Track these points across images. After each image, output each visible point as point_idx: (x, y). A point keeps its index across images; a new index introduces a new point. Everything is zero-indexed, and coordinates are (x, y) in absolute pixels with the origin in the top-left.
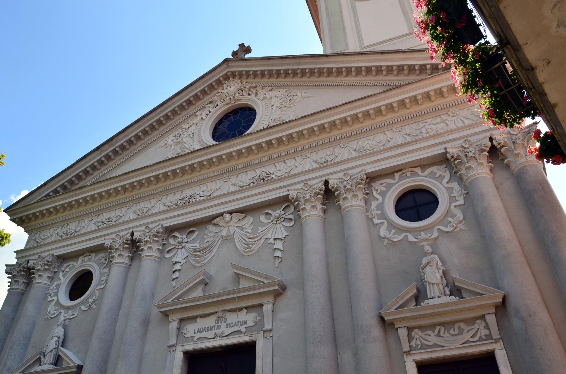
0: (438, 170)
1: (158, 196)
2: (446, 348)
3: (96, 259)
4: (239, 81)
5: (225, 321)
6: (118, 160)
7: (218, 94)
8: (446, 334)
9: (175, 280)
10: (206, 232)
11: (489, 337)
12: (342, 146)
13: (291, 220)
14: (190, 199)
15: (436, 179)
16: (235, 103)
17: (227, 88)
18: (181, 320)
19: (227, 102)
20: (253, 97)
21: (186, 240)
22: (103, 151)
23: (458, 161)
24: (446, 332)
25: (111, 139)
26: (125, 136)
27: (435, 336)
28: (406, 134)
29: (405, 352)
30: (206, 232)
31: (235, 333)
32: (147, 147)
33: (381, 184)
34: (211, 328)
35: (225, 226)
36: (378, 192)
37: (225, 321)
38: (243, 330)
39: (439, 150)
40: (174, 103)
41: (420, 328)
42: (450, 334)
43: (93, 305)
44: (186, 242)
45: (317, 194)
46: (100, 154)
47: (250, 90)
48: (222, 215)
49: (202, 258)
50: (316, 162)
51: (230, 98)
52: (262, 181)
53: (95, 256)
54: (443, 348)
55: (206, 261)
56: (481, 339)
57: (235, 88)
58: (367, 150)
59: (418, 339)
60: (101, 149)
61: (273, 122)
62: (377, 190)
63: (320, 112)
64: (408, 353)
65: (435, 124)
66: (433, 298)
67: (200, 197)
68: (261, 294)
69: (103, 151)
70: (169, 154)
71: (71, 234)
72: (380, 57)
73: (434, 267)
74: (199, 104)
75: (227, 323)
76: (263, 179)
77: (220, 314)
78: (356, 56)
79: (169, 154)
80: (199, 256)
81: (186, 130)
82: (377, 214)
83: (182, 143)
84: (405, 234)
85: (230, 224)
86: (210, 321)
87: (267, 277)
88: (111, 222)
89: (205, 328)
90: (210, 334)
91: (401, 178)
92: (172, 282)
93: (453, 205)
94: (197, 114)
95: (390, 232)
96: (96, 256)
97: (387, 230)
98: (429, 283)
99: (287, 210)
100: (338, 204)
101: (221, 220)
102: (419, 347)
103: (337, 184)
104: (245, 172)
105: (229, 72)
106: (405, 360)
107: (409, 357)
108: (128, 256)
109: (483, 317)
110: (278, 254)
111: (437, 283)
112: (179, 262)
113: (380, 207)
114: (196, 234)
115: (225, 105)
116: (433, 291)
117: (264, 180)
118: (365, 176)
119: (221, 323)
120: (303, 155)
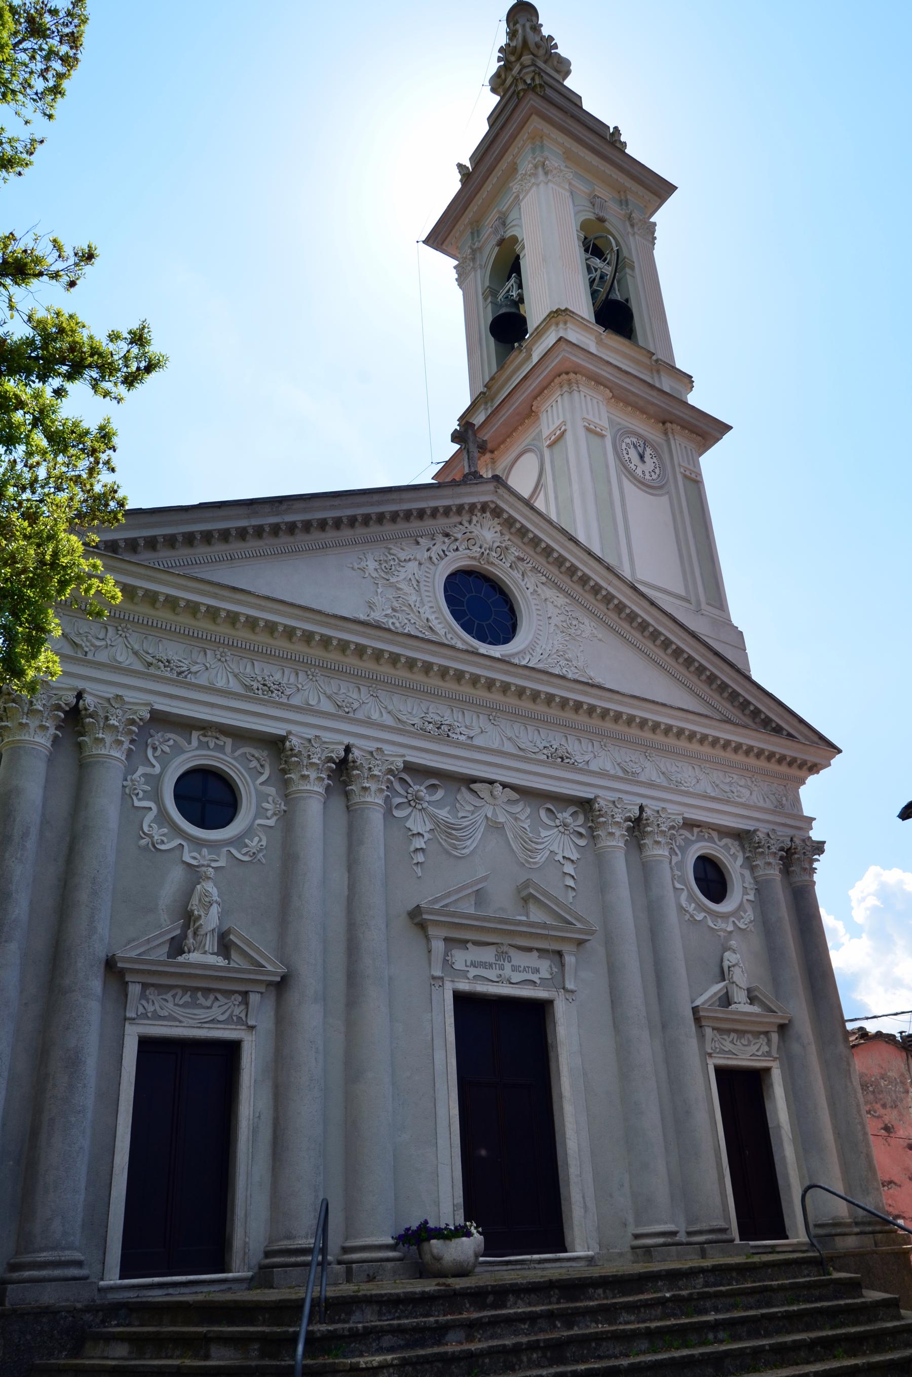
1: (374, 686)
4: (498, 528)
6: (267, 544)
7: (460, 526)
8: (738, 1043)
11: (768, 1054)
13: (580, 835)
18: (446, 940)
20: (516, 575)
21: (427, 798)
23: (14, 705)
30: (459, 797)
31: (527, 982)
32: (325, 547)
34: (491, 965)
36: (156, 755)
38: (538, 981)
39: (277, 729)
48: (491, 782)
52: (560, 760)
56: (763, 1055)
63: (653, 702)
64: (710, 1055)
66: (739, 1003)
68: (563, 939)
70: (376, 597)
71: (179, 674)
76: (562, 758)
77: (505, 949)
78: (685, 633)
80: (457, 839)
84: (703, 914)
86: (488, 955)
87: (579, 919)
90: (492, 974)
91: (203, 745)
93: (259, 821)
95: (690, 905)
98: (737, 985)
102: (718, 1050)
103: (95, 707)
104: (525, 725)
105: (492, 502)
109: (766, 1033)
110: (571, 883)
114: (440, 794)
117: (563, 759)
118: (681, 821)
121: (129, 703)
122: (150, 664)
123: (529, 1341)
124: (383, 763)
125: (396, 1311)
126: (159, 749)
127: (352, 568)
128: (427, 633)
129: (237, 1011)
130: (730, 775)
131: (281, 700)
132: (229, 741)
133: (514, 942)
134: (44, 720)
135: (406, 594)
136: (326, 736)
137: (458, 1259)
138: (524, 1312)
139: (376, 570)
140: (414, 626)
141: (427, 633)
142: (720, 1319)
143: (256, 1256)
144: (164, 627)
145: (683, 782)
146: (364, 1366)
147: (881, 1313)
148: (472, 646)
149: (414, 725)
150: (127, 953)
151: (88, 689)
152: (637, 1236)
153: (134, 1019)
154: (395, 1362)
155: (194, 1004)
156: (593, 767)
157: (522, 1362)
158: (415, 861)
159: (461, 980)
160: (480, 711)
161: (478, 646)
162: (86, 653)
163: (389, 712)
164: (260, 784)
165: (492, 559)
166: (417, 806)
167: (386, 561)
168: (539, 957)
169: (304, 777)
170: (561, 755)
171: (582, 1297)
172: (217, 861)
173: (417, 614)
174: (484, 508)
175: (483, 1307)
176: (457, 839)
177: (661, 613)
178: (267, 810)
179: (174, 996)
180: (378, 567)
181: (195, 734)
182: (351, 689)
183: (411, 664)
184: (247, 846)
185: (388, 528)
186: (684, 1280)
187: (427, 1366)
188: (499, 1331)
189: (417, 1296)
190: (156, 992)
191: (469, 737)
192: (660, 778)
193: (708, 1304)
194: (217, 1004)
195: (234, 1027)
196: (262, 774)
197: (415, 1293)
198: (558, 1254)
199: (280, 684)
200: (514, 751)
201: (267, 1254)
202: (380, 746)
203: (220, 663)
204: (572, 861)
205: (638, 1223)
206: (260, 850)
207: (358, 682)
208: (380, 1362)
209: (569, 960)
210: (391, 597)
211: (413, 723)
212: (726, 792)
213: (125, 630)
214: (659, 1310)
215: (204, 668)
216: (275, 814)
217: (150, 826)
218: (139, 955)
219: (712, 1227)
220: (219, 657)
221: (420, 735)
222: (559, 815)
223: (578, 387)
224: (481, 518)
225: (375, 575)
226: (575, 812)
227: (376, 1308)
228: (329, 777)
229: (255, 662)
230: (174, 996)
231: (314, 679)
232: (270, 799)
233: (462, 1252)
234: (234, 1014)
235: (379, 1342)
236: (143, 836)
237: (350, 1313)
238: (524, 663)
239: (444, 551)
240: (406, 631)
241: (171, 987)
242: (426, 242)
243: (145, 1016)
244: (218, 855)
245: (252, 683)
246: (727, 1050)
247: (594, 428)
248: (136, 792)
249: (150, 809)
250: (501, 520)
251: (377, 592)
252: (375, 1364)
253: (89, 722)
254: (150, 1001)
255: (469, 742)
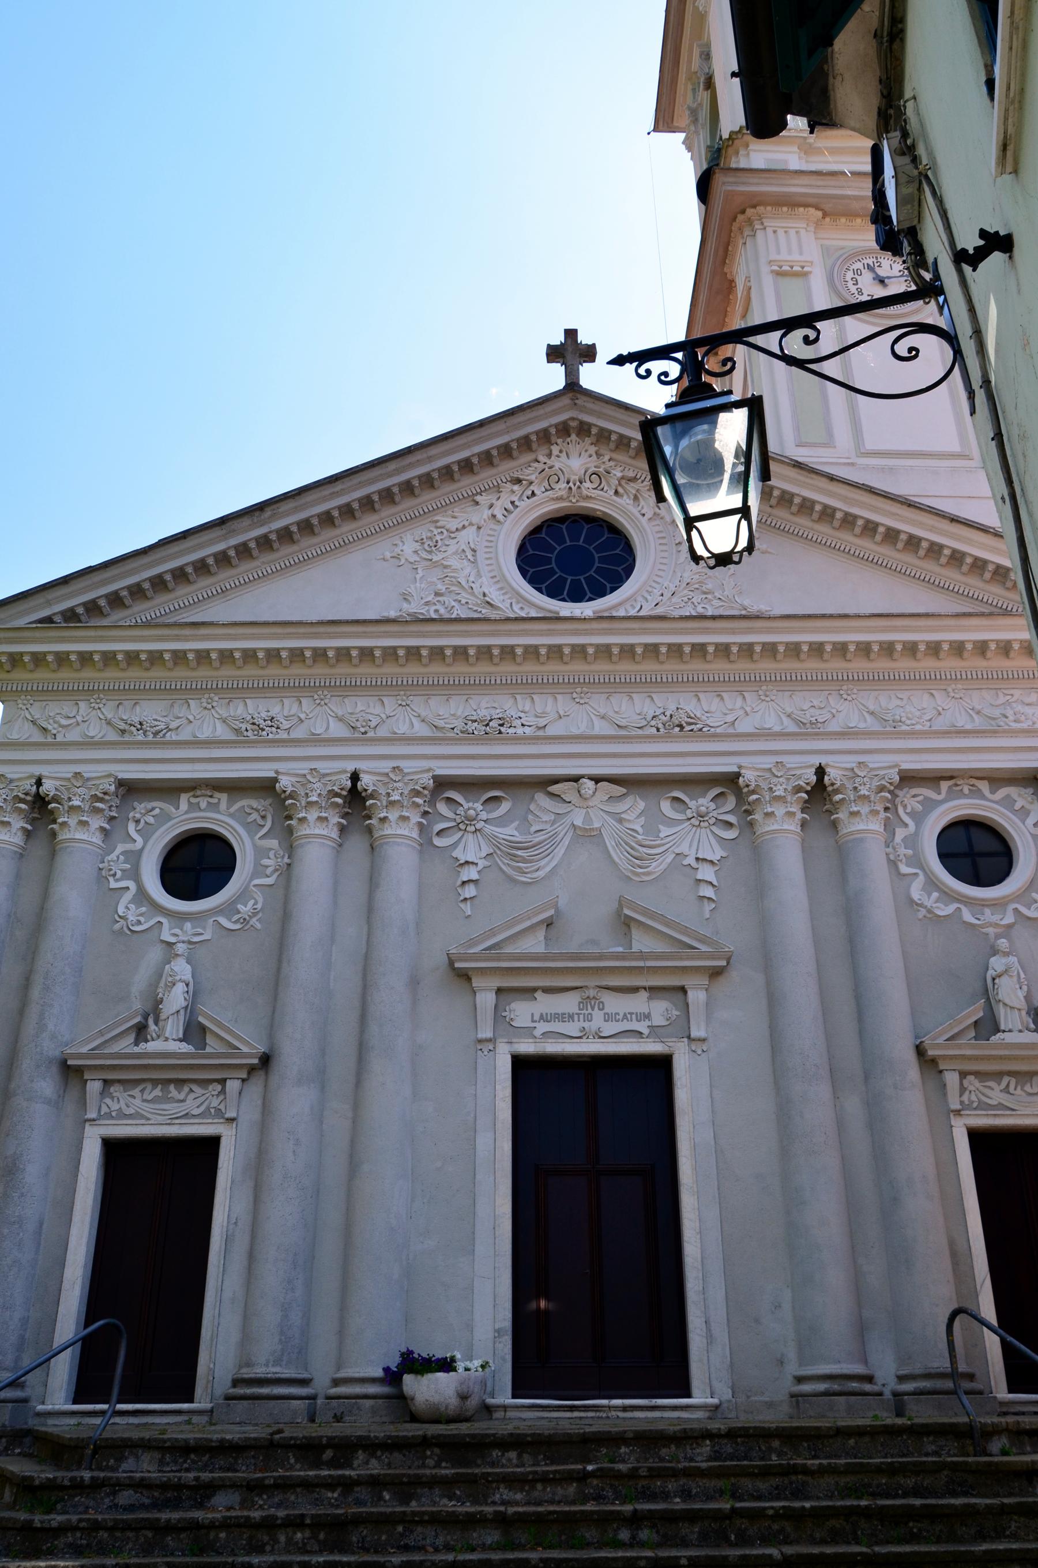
0: (1020, 795)
1: (402, 693)
2: (1019, 1113)
3: (232, 810)
4: (592, 449)
5: (601, 1007)
6: (264, 563)
7: (536, 465)
8: (1019, 1091)
9: (469, 902)
10: (532, 807)
12: (845, 696)
13: (729, 825)
14: (502, 725)
15: (1015, 812)
16: (577, 501)
17: (558, 456)
18: (499, 991)
19: (560, 493)
20: (626, 501)
21: (484, 815)
22: (234, 531)
24: (1019, 1088)
25: (260, 507)
26: (297, 510)
27: (1001, 1091)
28: (973, 709)
29: (952, 1111)
30: (532, 807)
31: (628, 1034)
32: (344, 545)
33: (914, 796)
34: (571, 1017)
35: (577, 805)
37: (601, 1007)
39: (263, 771)
40: (430, 459)
41: (977, 1074)
42: (1025, 1091)
43: (254, 920)
44: (485, 821)
45: (798, 789)
46: (225, 537)
47: (620, 484)
48: (576, 779)
49: (532, 866)
50: (789, 716)
51: (570, 488)
52: (677, 729)
53: (228, 801)
54: (1014, 1113)
55: (541, 874)
57: (582, 465)
58: (900, 721)
59: (973, 1092)
60: (228, 524)
61: (685, 588)
62: (905, 807)
63: (823, 616)
64: (958, 1113)
65: (1027, 705)
66: (1010, 1031)
67: (523, 725)
68: (684, 970)
69: (233, 532)
70: (412, 586)
71: (156, 734)
72: (945, 525)
73: (1015, 979)
74: (486, 476)
75: (606, 1011)
76: (681, 727)
78: (896, 504)
79: (412, 586)
80: (524, 860)
81: (453, 535)
82: (905, 855)
83: (446, 567)
84: (955, 906)
85: (591, 804)
86: (568, 1003)
87: (703, 940)
88: (278, 728)
89: (558, 1014)
90: (571, 1028)
91: (193, 807)
92: (462, 905)
94: (478, 498)
95: (929, 895)
96: (231, 803)
97: (923, 889)
98: (1005, 1005)
99: (720, 801)
100: (834, 819)
101: (569, 789)
102: (975, 1105)
105: (573, 419)
106: (953, 1123)
107: (958, 1119)
108: (338, 822)
110: (709, 892)
111: (1019, 1007)
112: (473, 863)
113: (912, 841)
114: (505, 807)
115: (553, 499)
116: (1007, 1019)
119: (593, 1010)
120: (761, 693)
121: (408, 774)
122: (123, 731)
123: (288, 1515)
124: (406, 784)
125: (185, 1462)
126: (142, 821)
127: (384, 559)
128: (484, 611)
129: (215, 1103)
130: (1006, 692)
131: (277, 737)
132: (224, 797)
133: (604, 983)
134: (789, 805)
135: (455, 570)
136: (323, 766)
137: (431, 1399)
138: (330, 1476)
139: (416, 552)
140: (466, 607)
141: (484, 611)
142: (642, 1511)
143: (223, 1385)
144: (649, 680)
145: (903, 719)
146: (39, 1525)
147: (1013, 1525)
148: (550, 611)
149: (453, 729)
150: (81, 1048)
151: (44, 774)
152: (800, 1380)
153: (94, 1120)
154: (83, 1525)
155: (166, 1099)
156: (743, 727)
157: (276, 1541)
158: (462, 898)
159: (522, 1040)
160: (532, 692)
161: (557, 609)
162: (55, 735)
163: (423, 721)
164: (259, 838)
165: (585, 492)
166: (468, 829)
167: (430, 538)
168: (650, 998)
169: (769, 815)
170: (677, 722)
171: (479, 1462)
172: (202, 934)
173: (470, 591)
174: (564, 430)
175: (317, 1464)
176: (524, 860)
177: (847, 487)
178: (267, 867)
179: (142, 1091)
180: (418, 548)
181: (184, 798)
182: (372, 704)
183: (817, 649)
184: (239, 912)
185: (427, 499)
186: (673, 1447)
187: (130, 1534)
188: (293, 1498)
189: (214, 1444)
190: (122, 1088)
191: (539, 728)
192: (865, 721)
193: (671, 1486)
194: (192, 1096)
195: (210, 1121)
196: (263, 826)
197: (211, 1441)
198: (654, 1401)
199: (273, 718)
200: (612, 731)
201: (236, 1383)
202: (395, 763)
203: (206, 712)
204: (711, 862)
205: (802, 1362)
206: (255, 914)
207: (379, 693)
208: (60, 1523)
209: (697, 997)
210: (435, 579)
211: (452, 726)
212: (994, 719)
213: (210, 700)
214: (572, 1489)
215: (186, 721)
216: (276, 870)
217: (127, 908)
218: (92, 1050)
219: (928, 1371)
220: (205, 704)
221: (460, 739)
222: (692, 804)
223: (762, 224)
224: (565, 444)
225: (414, 558)
226: (722, 794)
227: (157, 1455)
228: (803, 810)
229: (699, 694)
230: (142, 1091)
231: (323, 703)
232: (271, 854)
233: (436, 1392)
234: (212, 1106)
235: (115, 1499)
236: (118, 919)
237: (121, 1459)
238: (632, 612)
239: (512, 503)
240: (453, 616)
241: (137, 1082)
242: (656, 129)
243: (109, 1116)
244: (204, 928)
245: (241, 725)
246: (995, 1103)
247: (800, 269)
248: (112, 872)
249: (128, 888)
250: (593, 439)
251: (415, 578)
252: (54, 1524)
253: (289, 805)
254: (116, 1099)
255: (540, 733)
